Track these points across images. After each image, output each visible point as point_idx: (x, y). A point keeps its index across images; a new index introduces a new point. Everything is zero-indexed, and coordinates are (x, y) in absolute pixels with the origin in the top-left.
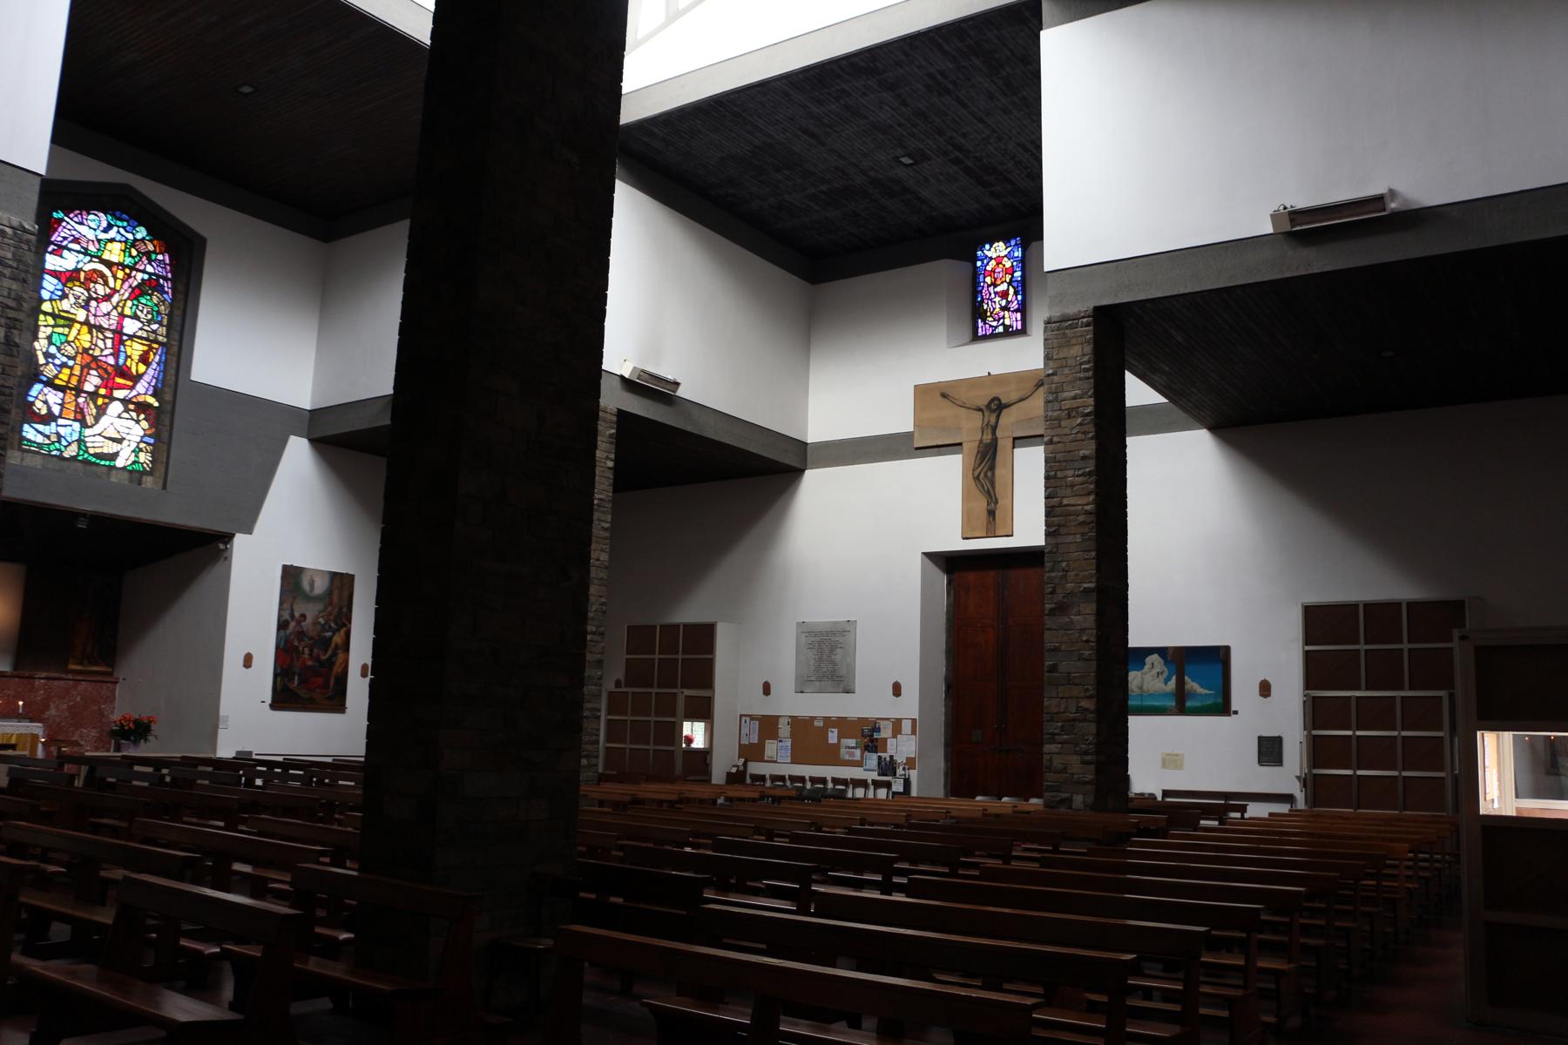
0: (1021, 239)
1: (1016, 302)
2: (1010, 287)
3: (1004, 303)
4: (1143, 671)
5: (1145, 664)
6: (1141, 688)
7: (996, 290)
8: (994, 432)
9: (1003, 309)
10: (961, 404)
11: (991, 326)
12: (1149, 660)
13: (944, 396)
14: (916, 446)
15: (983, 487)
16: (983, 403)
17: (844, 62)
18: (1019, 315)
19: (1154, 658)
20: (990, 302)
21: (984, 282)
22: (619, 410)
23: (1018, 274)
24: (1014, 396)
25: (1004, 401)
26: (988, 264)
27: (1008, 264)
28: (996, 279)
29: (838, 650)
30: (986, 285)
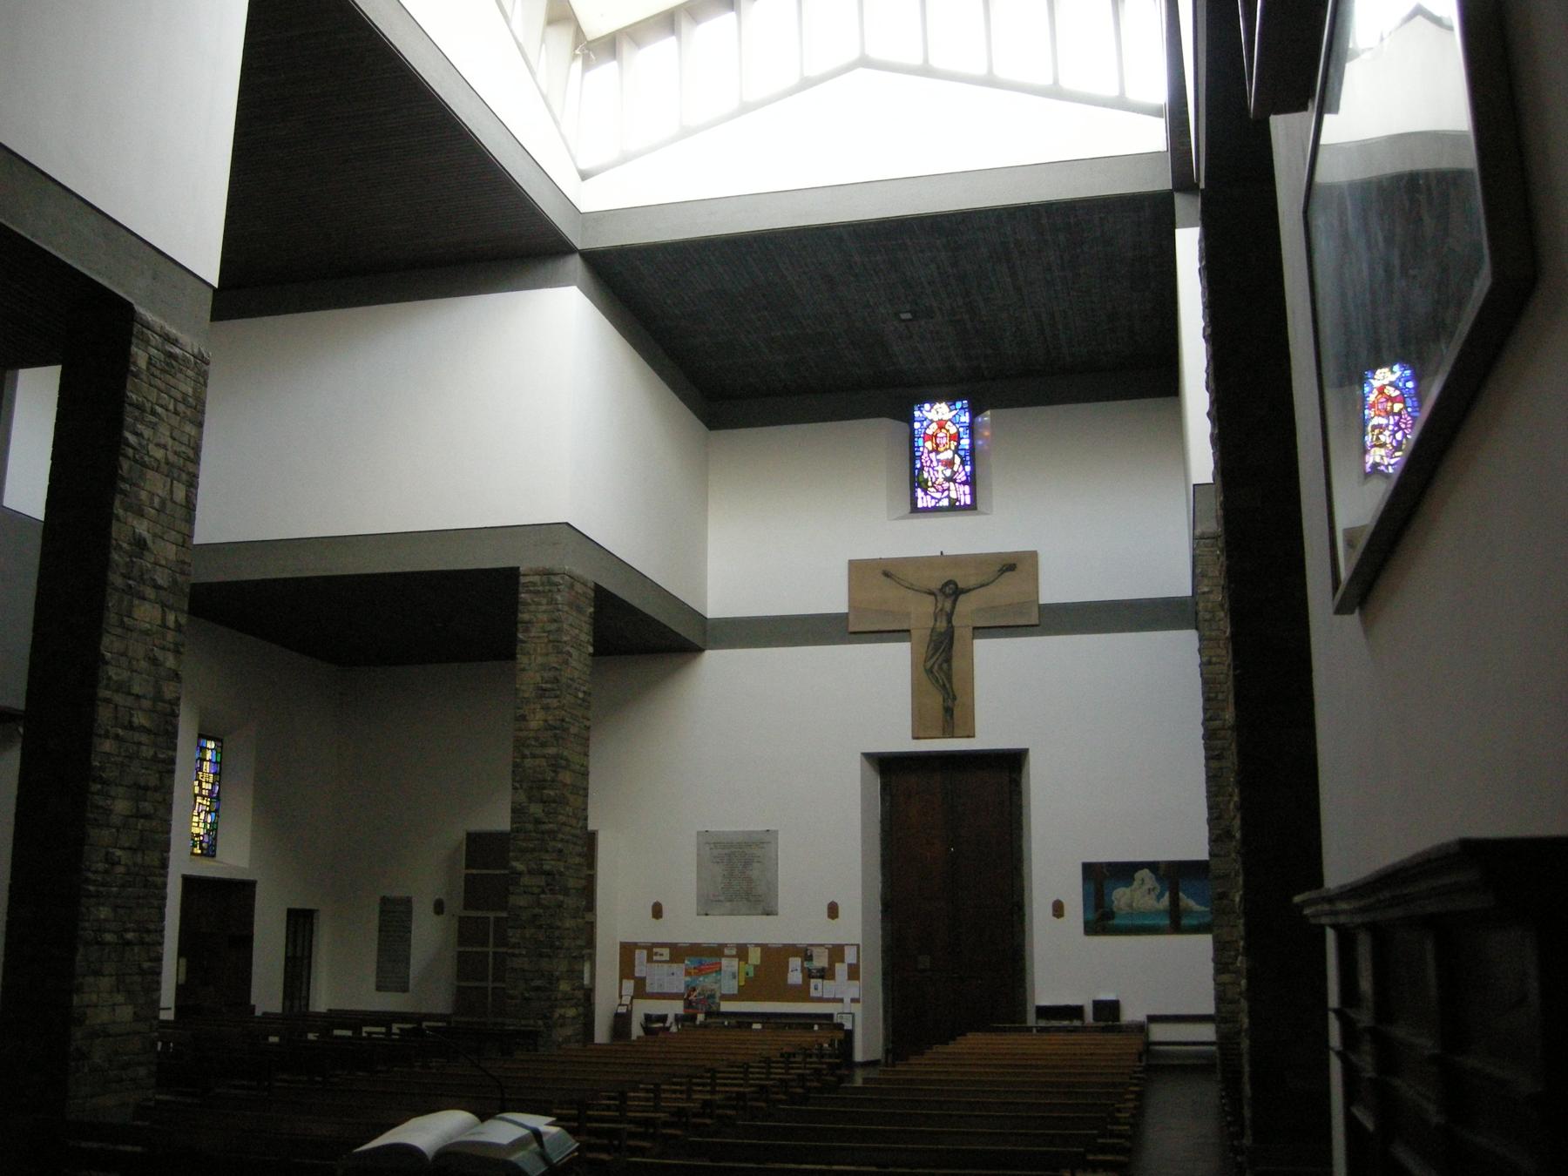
0: (968, 403)
1: (963, 473)
2: (956, 456)
3: (948, 473)
4: (1133, 887)
5: (1134, 880)
6: (1130, 906)
7: (940, 457)
8: (949, 621)
9: (951, 479)
10: (909, 586)
11: (933, 498)
12: (1139, 875)
13: (887, 574)
14: (852, 629)
15: (937, 681)
16: (935, 585)
17: (990, 213)
18: (967, 489)
19: (1145, 873)
20: (931, 469)
21: (924, 447)
22: (596, 585)
23: (965, 443)
24: (972, 582)
25: (961, 585)
26: (928, 426)
27: (953, 430)
28: (938, 445)
29: (755, 865)
30: (926, 451)
